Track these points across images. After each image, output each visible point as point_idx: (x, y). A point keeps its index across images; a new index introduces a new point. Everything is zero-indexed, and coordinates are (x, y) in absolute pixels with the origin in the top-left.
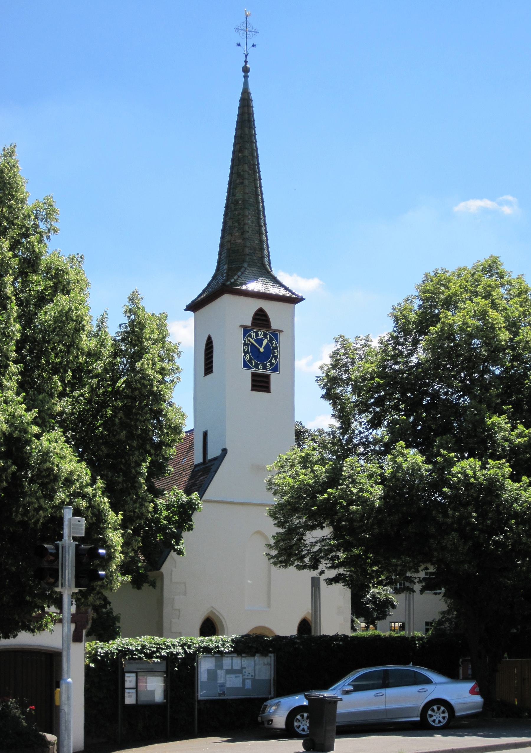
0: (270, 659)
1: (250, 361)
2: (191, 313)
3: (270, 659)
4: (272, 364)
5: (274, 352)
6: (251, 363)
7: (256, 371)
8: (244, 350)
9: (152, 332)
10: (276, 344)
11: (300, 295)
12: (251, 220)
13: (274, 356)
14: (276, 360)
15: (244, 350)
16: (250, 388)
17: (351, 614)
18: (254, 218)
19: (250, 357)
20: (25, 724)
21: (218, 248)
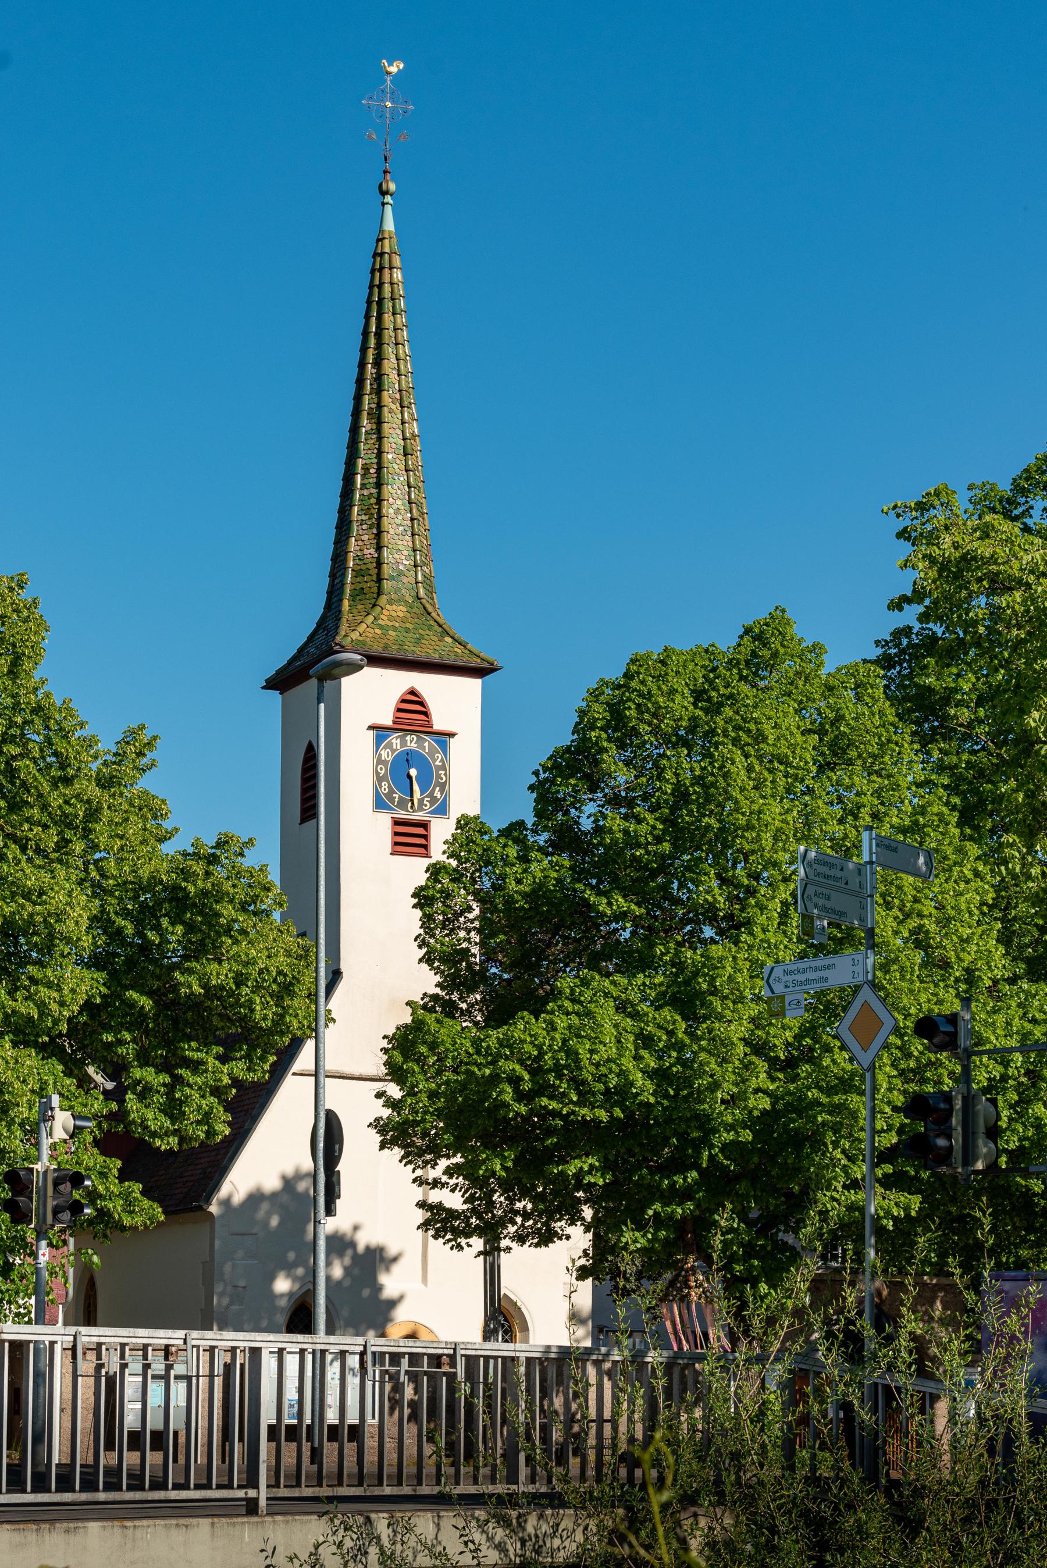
0: (337, 1422)
1: (390, 795)
2: (276, 694)
3: (337, 1422)
4: (433, 800)
5: (439, 776)
6: (392, 800)
7: (402, 815)
8: (378, 773)
9: (207, 1118)
10: (442, 761)
11: (490, 657)
12: (395, 506)
13: (438, 784)
14: (442, 791)
15: (378, 773)
16: (389, 847)
17: (560, 1347)
18: (399, 502)
19: (389, 787)
20: (1018, 1179)
21: (333, 532)
